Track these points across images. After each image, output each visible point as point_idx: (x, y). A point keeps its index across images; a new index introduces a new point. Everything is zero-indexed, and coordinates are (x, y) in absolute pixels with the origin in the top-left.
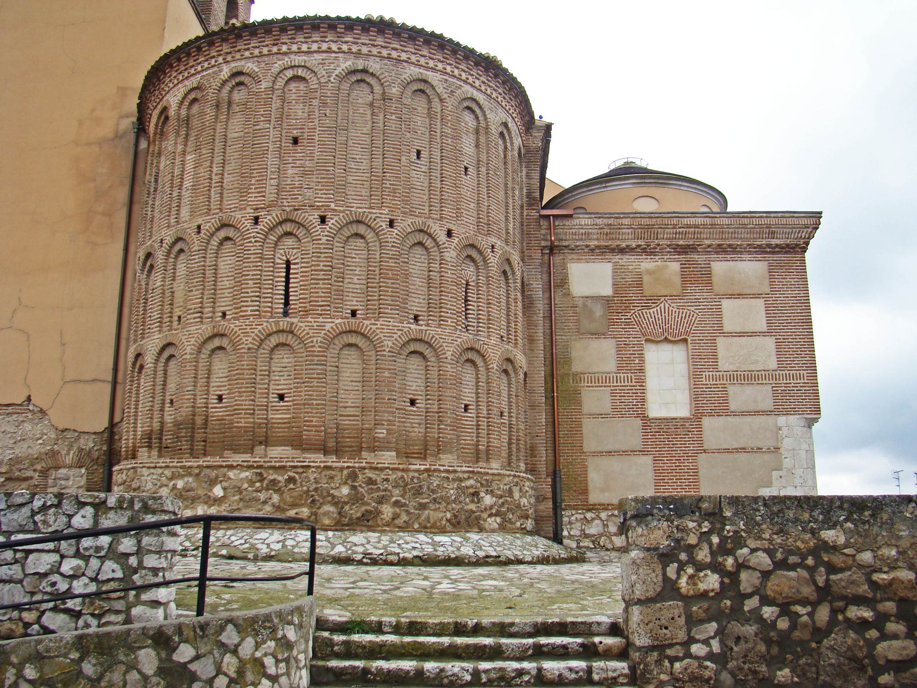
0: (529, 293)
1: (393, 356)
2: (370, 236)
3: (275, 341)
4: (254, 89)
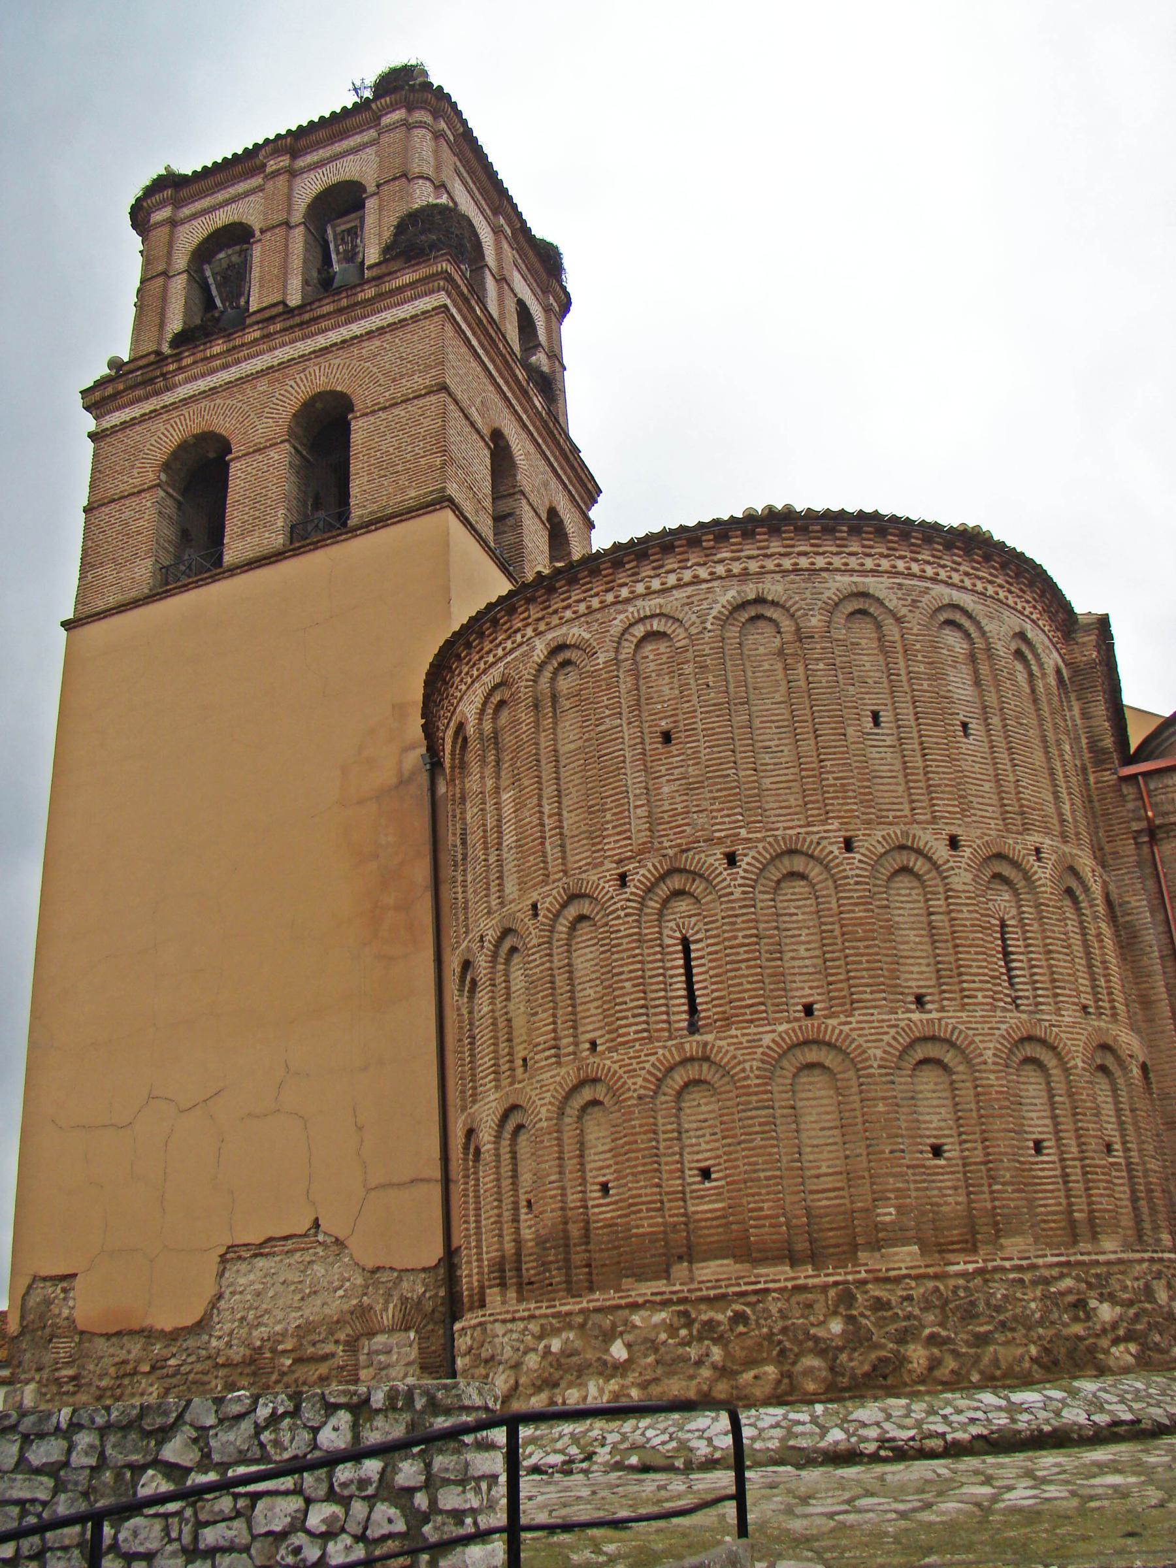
0: (1128, 918)
1: (887, 1074)
2: (815, 872)
3: (681, 1077)
4: (588, 668)
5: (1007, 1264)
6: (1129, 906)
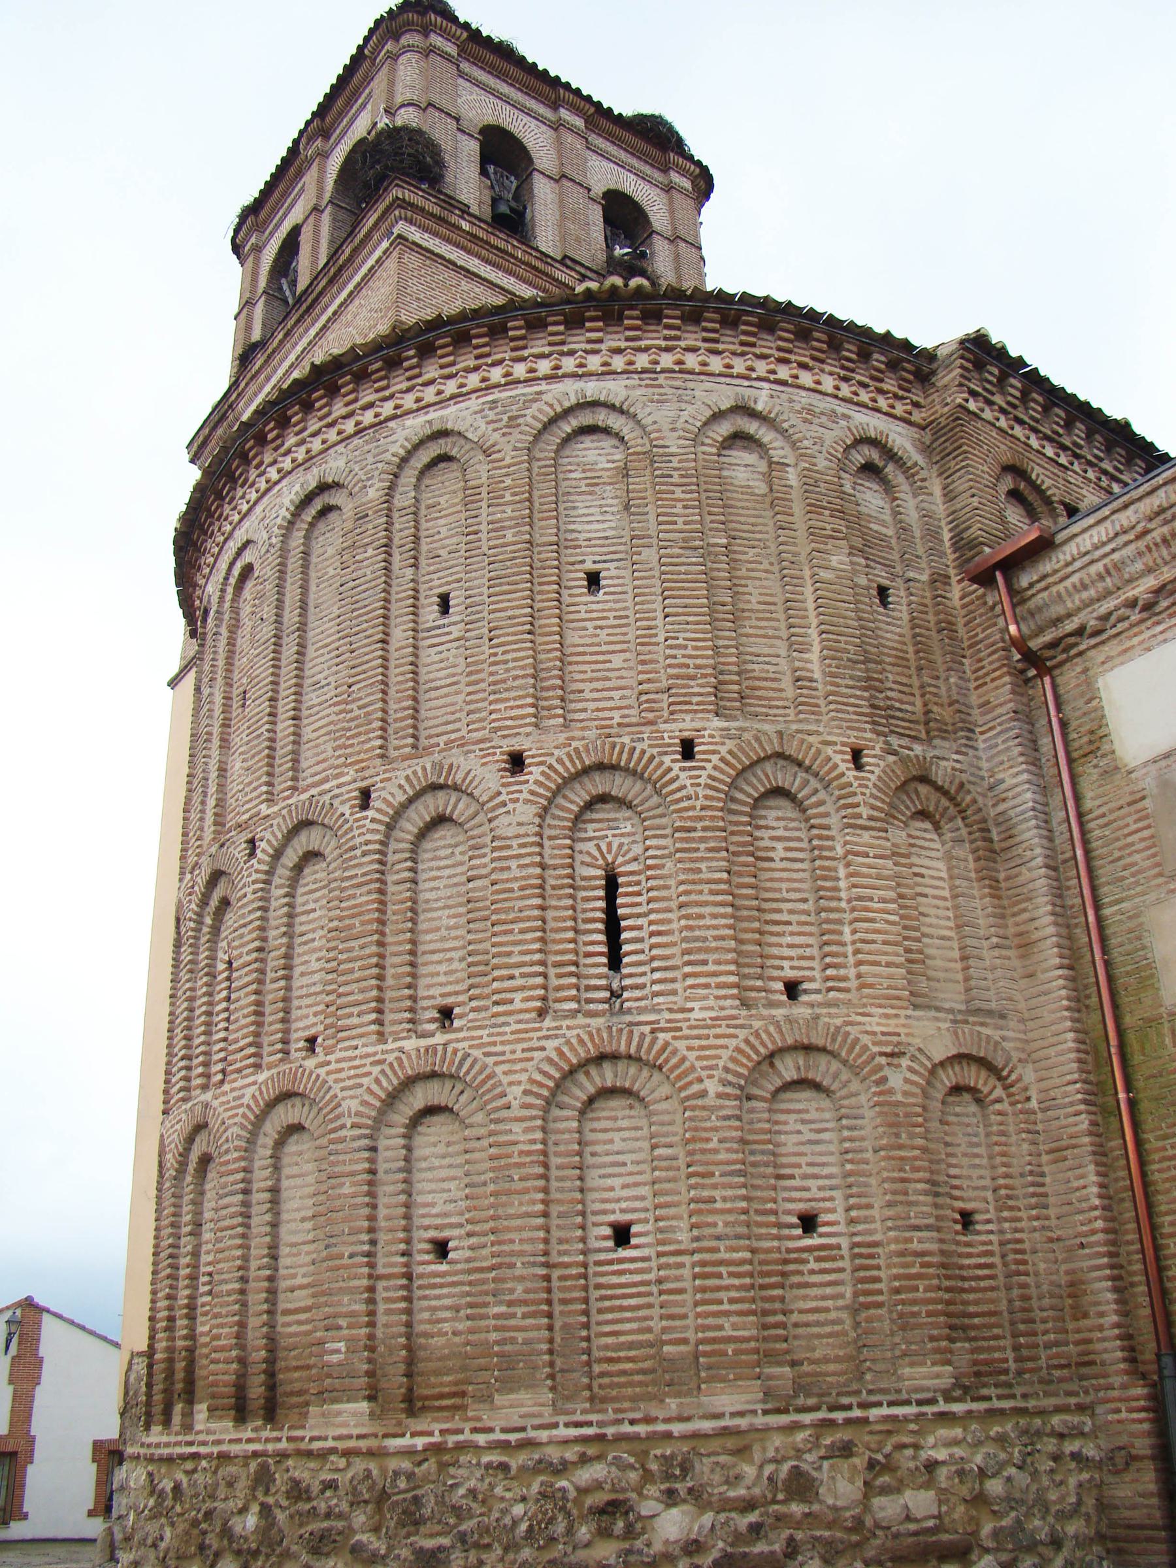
0: (1001, 807)
5: (481, 1439)
6: (1003, 787)
